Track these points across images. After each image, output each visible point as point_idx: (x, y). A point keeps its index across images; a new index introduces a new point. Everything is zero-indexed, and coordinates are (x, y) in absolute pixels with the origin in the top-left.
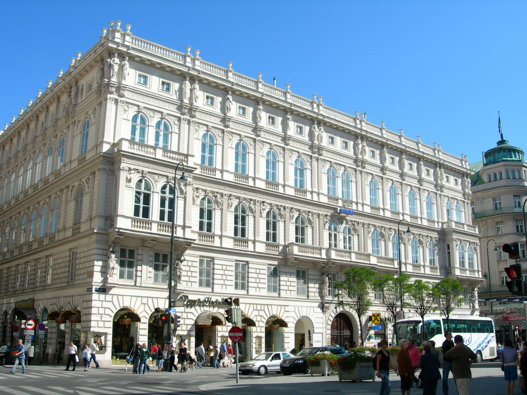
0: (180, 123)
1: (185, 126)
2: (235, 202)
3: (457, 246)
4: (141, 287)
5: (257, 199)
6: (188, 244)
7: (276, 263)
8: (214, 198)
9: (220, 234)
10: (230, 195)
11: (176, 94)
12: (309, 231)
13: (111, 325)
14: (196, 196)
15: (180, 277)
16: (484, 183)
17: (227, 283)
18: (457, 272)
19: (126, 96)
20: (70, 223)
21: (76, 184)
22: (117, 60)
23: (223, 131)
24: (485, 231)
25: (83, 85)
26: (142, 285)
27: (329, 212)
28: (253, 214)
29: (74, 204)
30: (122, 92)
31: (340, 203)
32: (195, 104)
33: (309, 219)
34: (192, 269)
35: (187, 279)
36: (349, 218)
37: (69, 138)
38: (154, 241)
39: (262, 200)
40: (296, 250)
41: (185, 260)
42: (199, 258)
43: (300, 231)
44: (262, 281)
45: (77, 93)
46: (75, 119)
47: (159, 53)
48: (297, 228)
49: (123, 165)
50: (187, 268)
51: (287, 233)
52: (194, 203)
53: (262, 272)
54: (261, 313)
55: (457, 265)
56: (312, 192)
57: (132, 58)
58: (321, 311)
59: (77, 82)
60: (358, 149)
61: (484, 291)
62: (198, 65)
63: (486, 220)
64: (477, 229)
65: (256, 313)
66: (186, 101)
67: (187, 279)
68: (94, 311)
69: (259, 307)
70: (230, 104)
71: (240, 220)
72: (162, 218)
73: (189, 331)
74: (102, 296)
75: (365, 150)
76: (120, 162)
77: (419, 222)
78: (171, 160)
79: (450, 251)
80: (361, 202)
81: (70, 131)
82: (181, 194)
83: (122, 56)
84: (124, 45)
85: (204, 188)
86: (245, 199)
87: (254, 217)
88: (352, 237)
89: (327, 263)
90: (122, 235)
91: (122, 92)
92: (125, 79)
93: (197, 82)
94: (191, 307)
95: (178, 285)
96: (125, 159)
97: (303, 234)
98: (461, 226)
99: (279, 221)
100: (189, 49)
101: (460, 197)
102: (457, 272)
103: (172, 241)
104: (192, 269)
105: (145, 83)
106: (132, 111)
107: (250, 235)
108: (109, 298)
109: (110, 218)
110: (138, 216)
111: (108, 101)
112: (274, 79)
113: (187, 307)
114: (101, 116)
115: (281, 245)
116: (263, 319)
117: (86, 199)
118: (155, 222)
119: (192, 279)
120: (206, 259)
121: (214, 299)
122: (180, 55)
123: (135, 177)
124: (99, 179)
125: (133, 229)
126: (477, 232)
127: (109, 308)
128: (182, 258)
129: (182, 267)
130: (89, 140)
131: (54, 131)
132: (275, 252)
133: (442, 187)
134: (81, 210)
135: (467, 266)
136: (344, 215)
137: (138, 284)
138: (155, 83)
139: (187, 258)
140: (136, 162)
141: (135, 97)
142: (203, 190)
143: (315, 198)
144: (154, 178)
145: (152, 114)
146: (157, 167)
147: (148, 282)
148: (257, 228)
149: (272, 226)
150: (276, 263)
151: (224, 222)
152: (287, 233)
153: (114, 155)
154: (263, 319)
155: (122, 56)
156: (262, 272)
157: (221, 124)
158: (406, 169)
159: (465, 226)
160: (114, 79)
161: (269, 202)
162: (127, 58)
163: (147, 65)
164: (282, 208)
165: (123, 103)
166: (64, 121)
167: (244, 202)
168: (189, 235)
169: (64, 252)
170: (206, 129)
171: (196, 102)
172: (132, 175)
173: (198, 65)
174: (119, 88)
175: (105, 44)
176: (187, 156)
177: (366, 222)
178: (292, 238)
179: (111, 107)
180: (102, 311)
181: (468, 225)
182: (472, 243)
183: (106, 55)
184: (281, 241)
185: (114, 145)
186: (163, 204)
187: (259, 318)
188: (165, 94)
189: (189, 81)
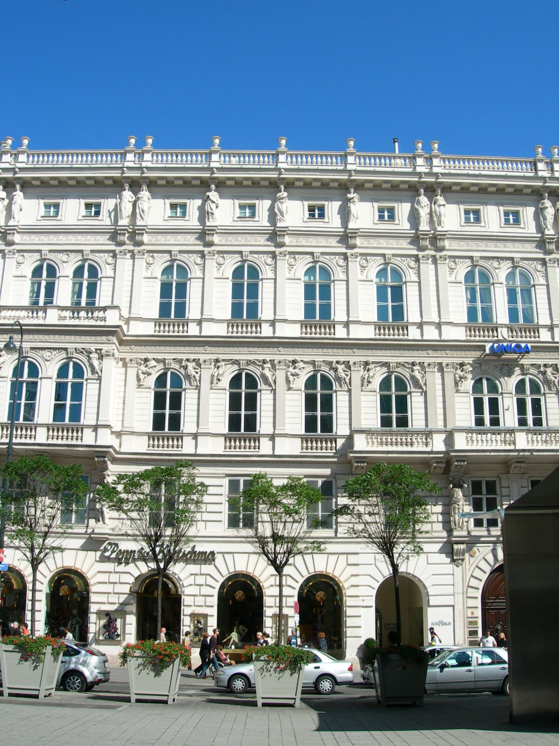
0: (347, 263)
1: (428, 268)
2: (379, 375)
7: (327, 471)
11: (110, 216)
13: (214, 601)
14: (293, 375)
19: (447, 248)
27: (469, 358)
28: (270, 385)
30: (440, 244)
32: (439, 229)
33: (413, 378)
36: (525, 361)
38: (523, 462)
42: (227, 479)
47: (78, 161)
52: (139, 386)
58: (448, 560)
60: (545, 219)
62: (352, 163)
70: (213, 206)
73: (123, 604)
82: (92, 374)
85: (160, 356)
88: (542, 399)
90: (464, 461)
91: (440, 244)
93: (145, 187)
94: (127, 563)
100: (540, 150)
105: (478, 220)
106: (463, 268)
110: (64, 421)
112: (395, 142)
113: (120, 563)
115: (342, 437)
120: (242, 479)
122: (526, 162)
125: (50, 441)
127: (370, 575)
132: (326, 451)
136: (515, 356)
138: (492, 216)
140: (78, 338)
142: (158, 361)
143: (431, 334)
146: (47, 337)
150: (327, 471)
162: (422, 190)
163: (510, 194)
165: (445, 259)
167: (250, 367)
170: (382, 261)
173: (438, 167)
184: (341, 428)
188: (249, 224)
189: (425, 195)
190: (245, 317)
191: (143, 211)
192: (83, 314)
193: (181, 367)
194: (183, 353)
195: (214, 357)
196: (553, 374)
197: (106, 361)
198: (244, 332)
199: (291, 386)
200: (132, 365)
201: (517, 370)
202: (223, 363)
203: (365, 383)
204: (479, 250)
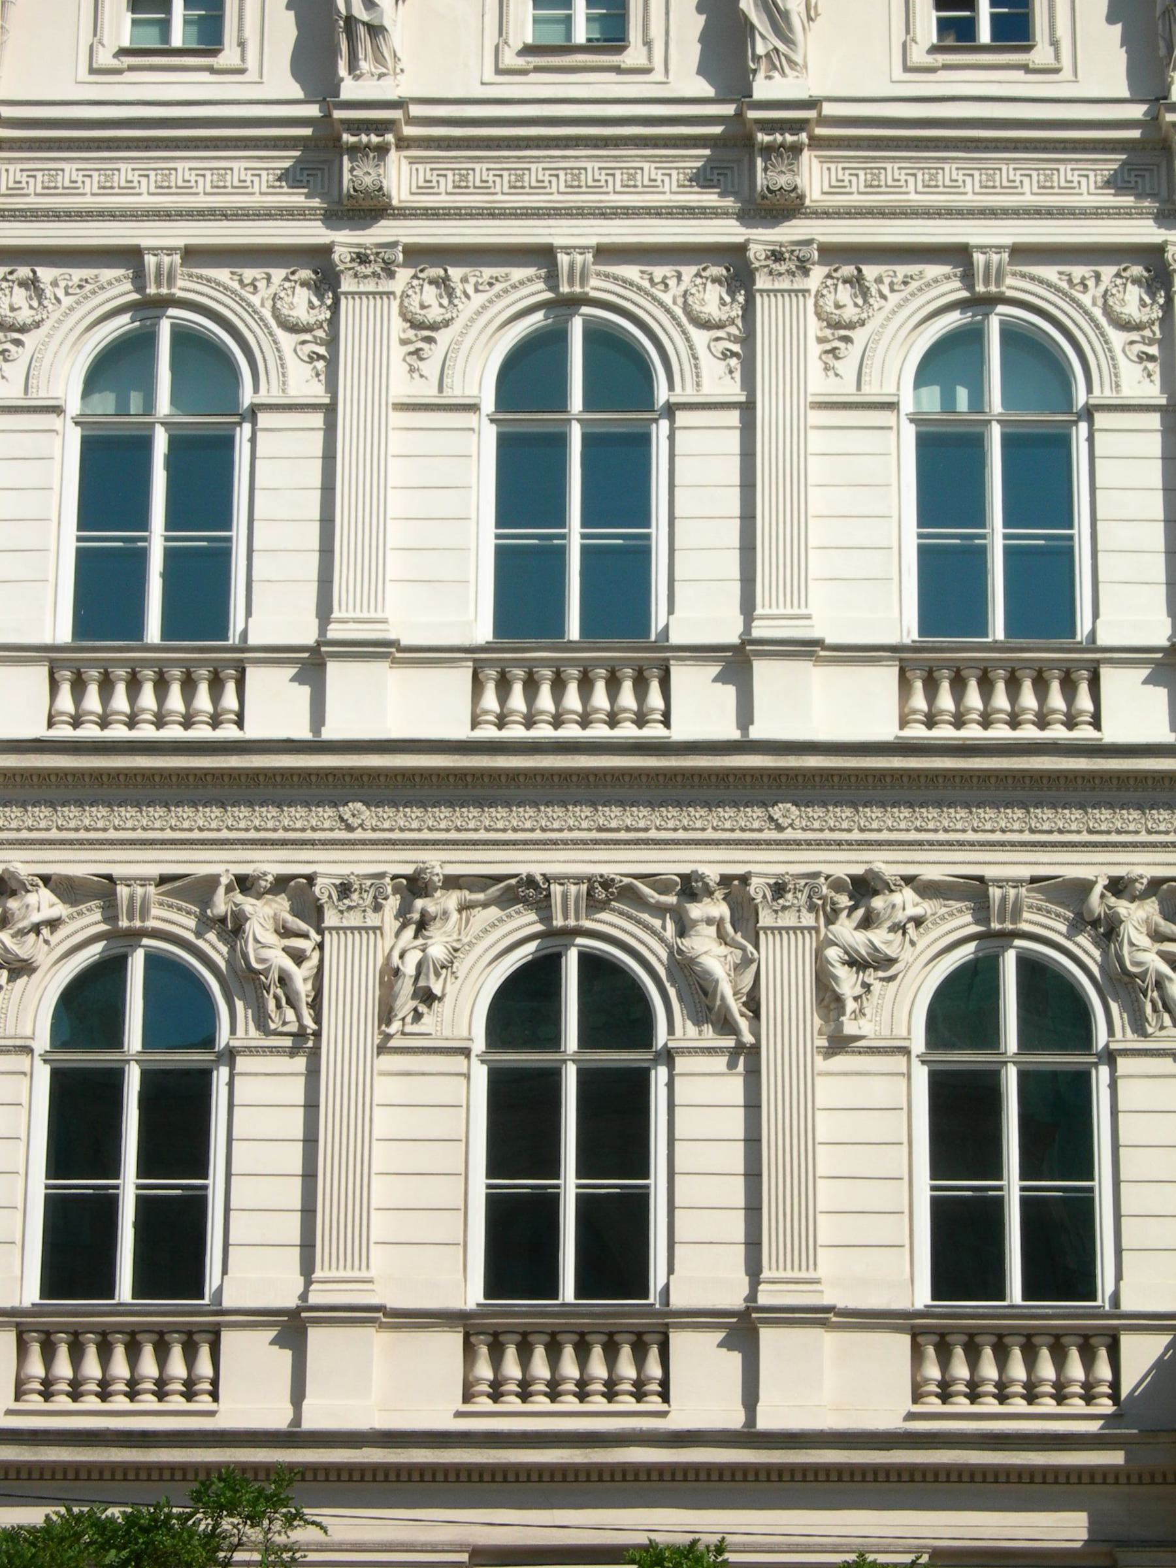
0: (335, 308)
8: (215, 947)
9: (734, 1299)
14: (856, 963)
23: (737, 270)
28: (726, 1025)
39: (845, 865)
86: (603, 893)
99: (1110, 1057)
142: (69, 890)
157: (298, 199)
167: (609, 921)
190: (574, 631)
193: (206, 923)
194: (221, 847)
195: (400, 863)
196: (285, 932)
198: (581, 717)
199: (850, 1027)
200: (788, 919)
202: (452, 900)
203: (405, 1004)
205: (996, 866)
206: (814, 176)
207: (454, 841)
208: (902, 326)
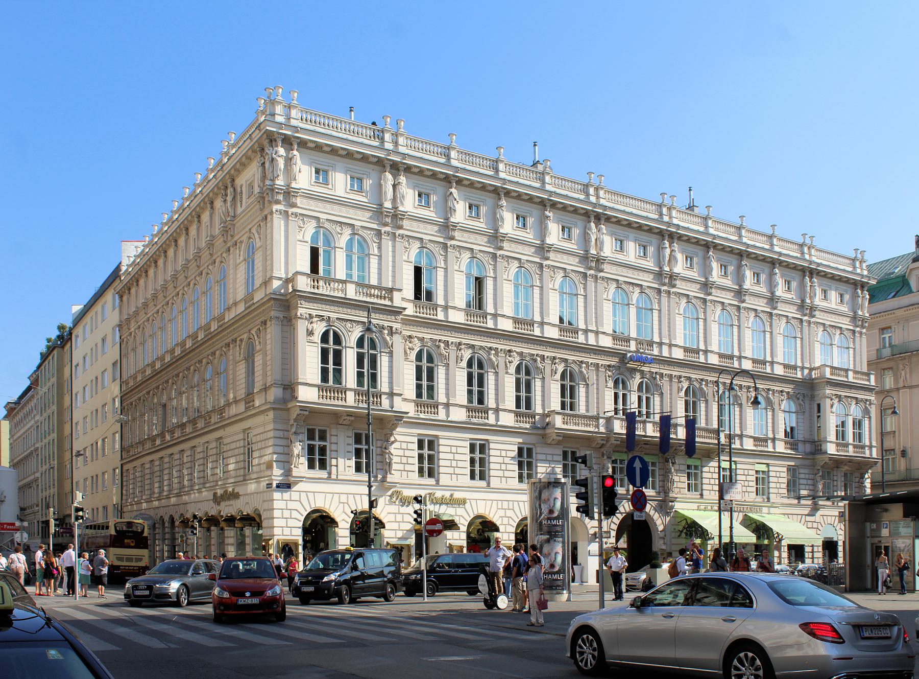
1: (387, 244)
2: (467, 354)
3: (832, 406)
4: (337, 479)
5: (500, 347)
6: (399, 418)
10: (460, 344)
12: (581, 391)
15: (390, 464)
16: (911, 292)
17: (458, 471)
18: (831, 449)
20: (241, 394)
21: (245, 336)
22: (282, 151)
24: (908, 376)
25: (241, 186)
26: (339, 477)
29: (244, 366)
31: (633, 346)
33: (581, 372)
34: (408, 453)
35: (401, 467)
37: (231, 267)
39: (508, 348)
40: (558, 422)
41: (396, 441)
43: (568, 393)
44: (460, 464)
45: (234, 198)
46: (235, 239)
48: (563, 387)
49: (301, 311)
50: (401, 453)
51: (548, 396)
52: (406, 359)
53: (460, 450)
54: (510, 513)
55: (832, 437)
56: (586, 331)
57: (303, 144)
59: (233, 180)
60: (664, 256)
61: (902, 477)
63: (910, 357)
64: (872, 377)
65: (501, 513)
66: (388, 205)
67: (401, 467)
68: (276, 513)
69: (505, 505)
71: (475, 381)
72: (360, 383)
74: (286, 495)
75: (676, 259)
76: (297, 308)
77: (768, 370)
78: (368, 300)
79: (821, 414)
80: (668, 342)
81: (231, 256)
83: (287, 142)
84: (289, 126)
85: (421, 335)
86: (481, 348)
87: (496, 373)
89: (608, 439)
92: (295, 179)
95: (389, 476)
96: (303, 302)
97: (572, 396)
98: (842, 373)
101: (845, 323)
102: (831, 449)
103: (368, 414)
104: (408, 453)
107: (491, 402)
108: (295, 496)
109: (290, 388)
111: (274, 215)
114: (268, 237)
115: (539, 414)
116: (511, 522)
117: (258, 360)
118: (351, 390)
119: (408, 467)
120: (478, 442)
121: (439, 494)
123: (320, 328)
124: (273, 332)
126: (873, 383)
128: (392, 439)
129: (392, 451)
130: (256, 272)
131: (211, 255)
133: (812, 309)
134: (253, 373)
135: (850, 438)
137: (334, 476)
139: (398, 438)
141: (313, 205)
143: (592, 340)
144: (345, 327)
145: (338, 229)
147: (347, 473)
148: (503, 389)
149: (524, 387)
151: (453, 383)
152: (548, 396)
153: (288, 297)
154: (511, 522)
155: (287, 142)
156: (460, 450)
158: (749, 283)
159: (851, 374)
160: (280, 182)
161: (518, 350)
164: (539, 359)
166: (222, 239)
167: (480, 352)
168: (399, 405)
169: (236, 434)
171: (402, 204)
172: (314, 325)
174: (289, 193)
175: (262, 127)
176: (391, 291)
177: (674, 373)
178: (555, 404)
179: (278, 223)
180: (287, 514)
181: (856, 372)
182: (862, 400)
183: (266, 143)
185: (287, 281)
186: (360, 364)
187: (505, 521)
191: (403, 197)
192: (321, 283)
194: (437, 335)
195: (458, 340)
197: (395, 337)
198: (476, 322)
201: (638, 376)
204: (325, 211)
205: (693, 376)
206: (457, 234)
207: (685, 372)
208: (310, 228)
